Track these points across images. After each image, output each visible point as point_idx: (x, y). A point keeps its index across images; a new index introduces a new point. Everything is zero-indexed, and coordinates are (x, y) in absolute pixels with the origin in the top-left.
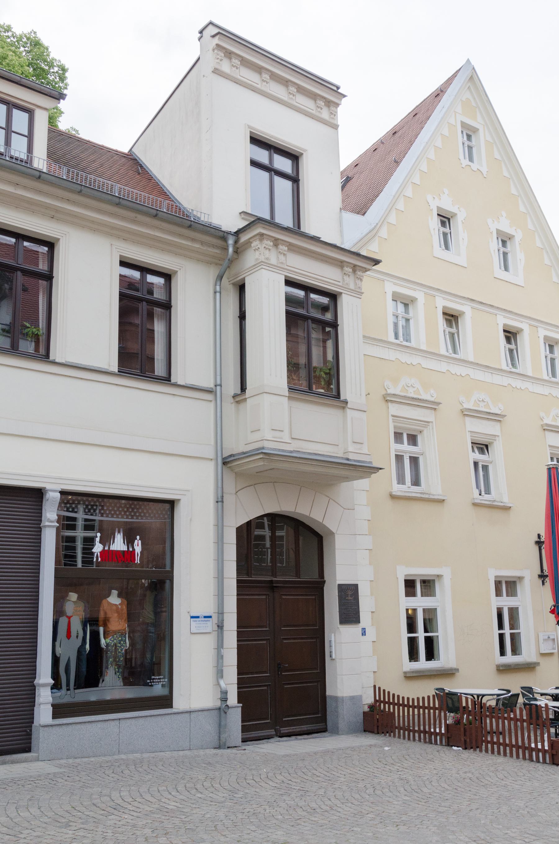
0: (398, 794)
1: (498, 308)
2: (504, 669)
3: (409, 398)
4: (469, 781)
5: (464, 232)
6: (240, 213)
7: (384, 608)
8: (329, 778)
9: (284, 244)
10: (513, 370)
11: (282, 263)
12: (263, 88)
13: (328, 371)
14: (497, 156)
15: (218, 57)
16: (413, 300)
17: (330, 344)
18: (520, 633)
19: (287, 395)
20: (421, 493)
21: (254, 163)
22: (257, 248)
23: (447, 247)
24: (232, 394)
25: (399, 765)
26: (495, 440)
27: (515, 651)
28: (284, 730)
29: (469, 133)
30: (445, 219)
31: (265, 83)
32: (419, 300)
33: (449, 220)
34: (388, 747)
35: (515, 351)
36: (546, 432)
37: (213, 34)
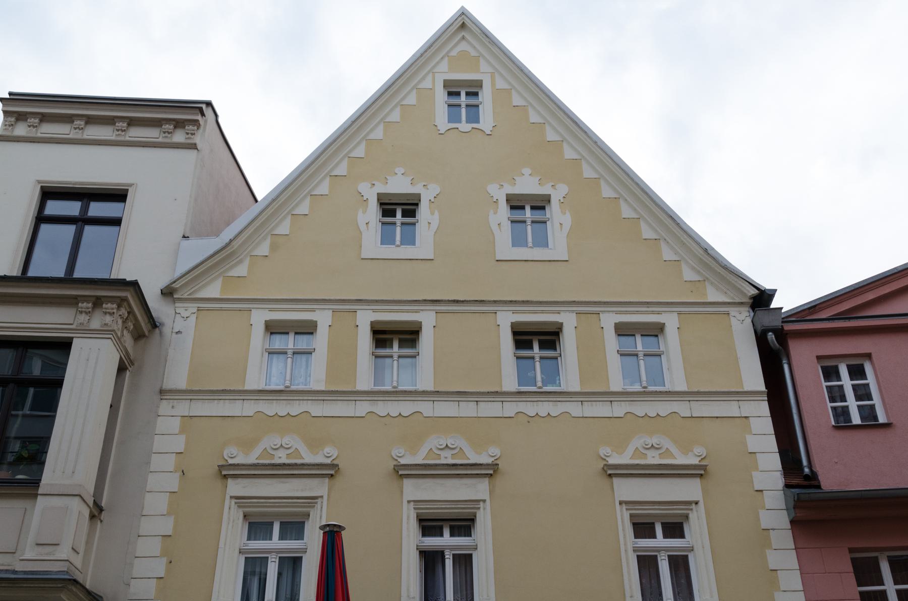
12: (79, 136)
26: (692, 510)
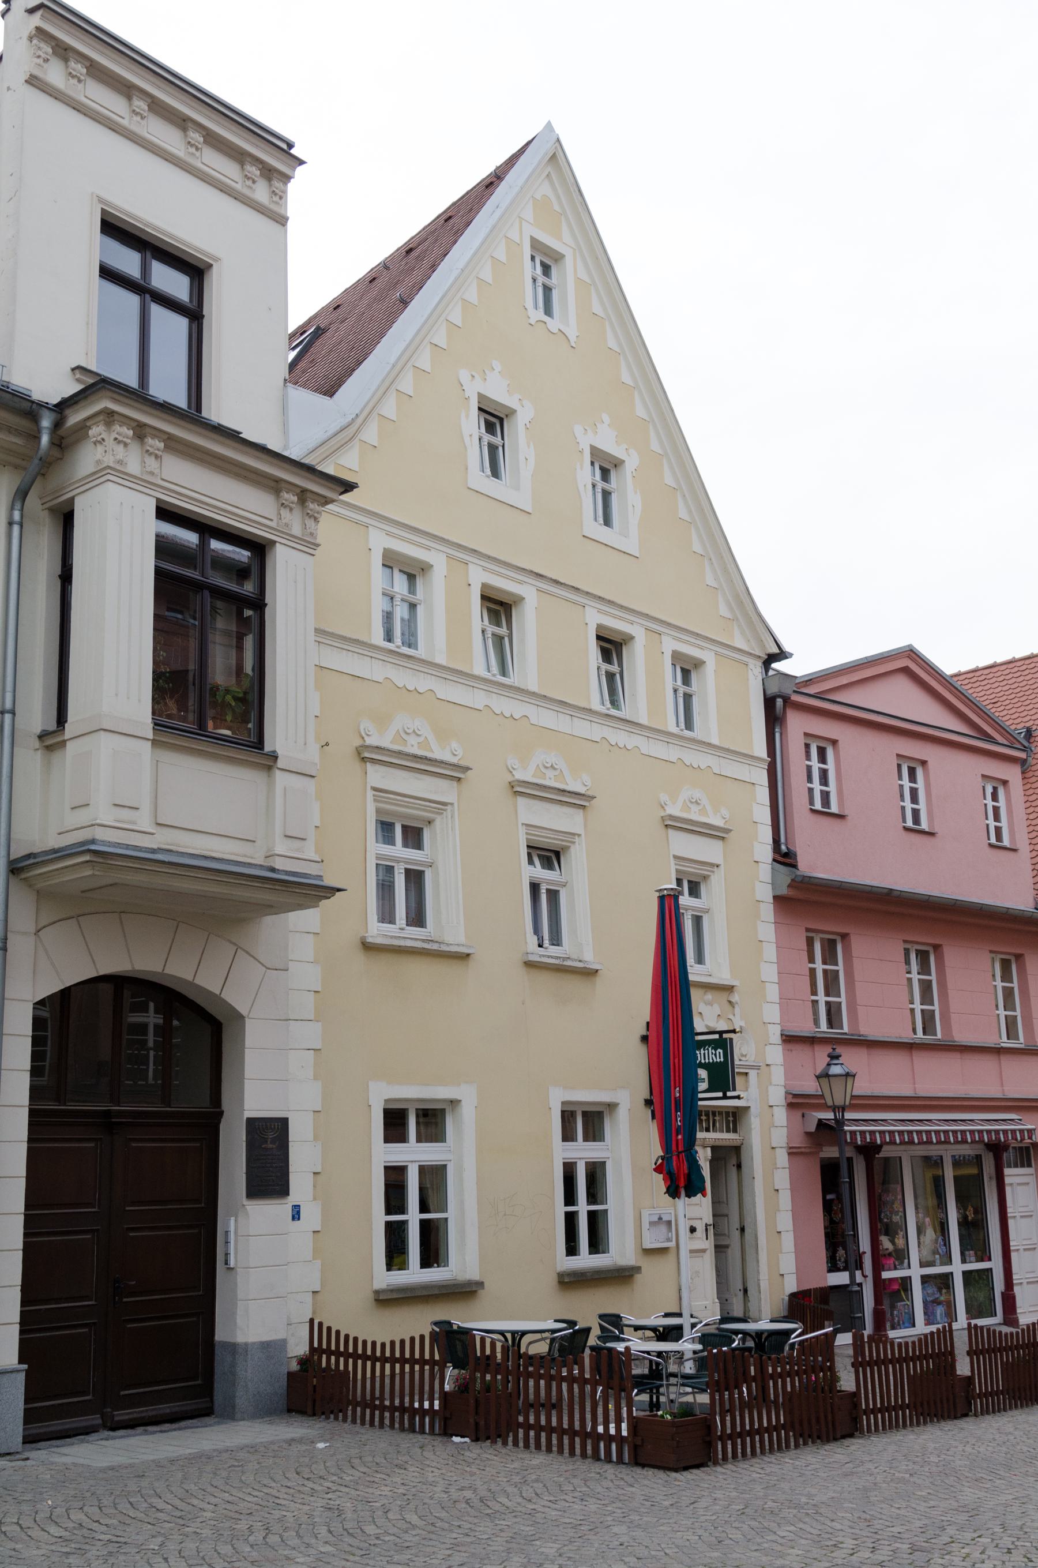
0: (313, 1541)
1: (587, 593)
2: (572, 1282)
3: (408, 755)
4: (464, 1505)
5: (529, 447)
6: (73, 370)
7: (337, 1165)
8: (179, 1514)
9: (157, 437)
10: (614, 712)
11: (152, 473)
12: (134, 127)
13: (241, 695)
14: (597, 308)
15: (40, 53)
16: (425, 568)
17: (249, 642)
18: (606, 1211)
19: (151, 736)
20: (423, 941)
21: (107, 273)
22: (99, 438)
23: (495, 473)
24: (38, 731)
25: (335, 1478)
27: (597, 1244)
28: (122, 1415)
29: (547, 262)
30: (494, 419)
31: (138, 118)
32: (435, 568)
33: (501, 420)
34: (325, 1441)
35: (618, 676)
36: (671, 831)
37: (30, 6)
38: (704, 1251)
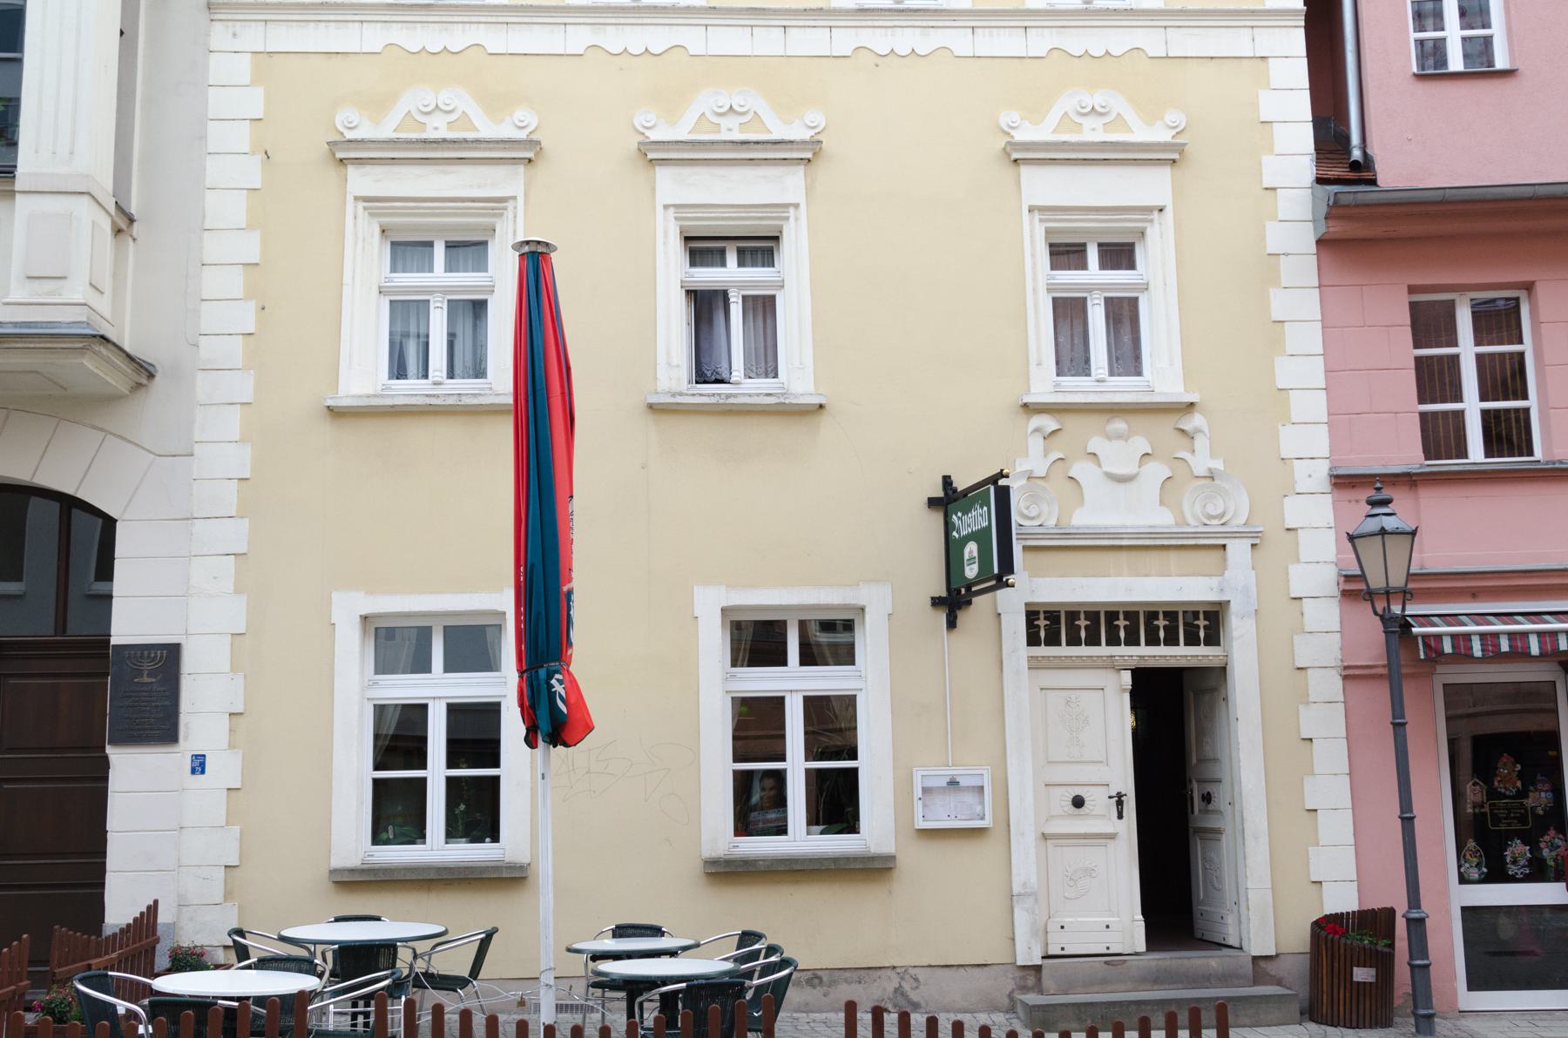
38: (1112, 837)
